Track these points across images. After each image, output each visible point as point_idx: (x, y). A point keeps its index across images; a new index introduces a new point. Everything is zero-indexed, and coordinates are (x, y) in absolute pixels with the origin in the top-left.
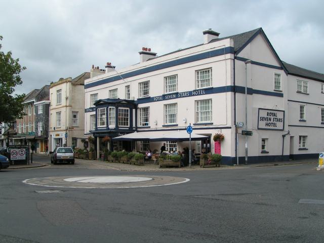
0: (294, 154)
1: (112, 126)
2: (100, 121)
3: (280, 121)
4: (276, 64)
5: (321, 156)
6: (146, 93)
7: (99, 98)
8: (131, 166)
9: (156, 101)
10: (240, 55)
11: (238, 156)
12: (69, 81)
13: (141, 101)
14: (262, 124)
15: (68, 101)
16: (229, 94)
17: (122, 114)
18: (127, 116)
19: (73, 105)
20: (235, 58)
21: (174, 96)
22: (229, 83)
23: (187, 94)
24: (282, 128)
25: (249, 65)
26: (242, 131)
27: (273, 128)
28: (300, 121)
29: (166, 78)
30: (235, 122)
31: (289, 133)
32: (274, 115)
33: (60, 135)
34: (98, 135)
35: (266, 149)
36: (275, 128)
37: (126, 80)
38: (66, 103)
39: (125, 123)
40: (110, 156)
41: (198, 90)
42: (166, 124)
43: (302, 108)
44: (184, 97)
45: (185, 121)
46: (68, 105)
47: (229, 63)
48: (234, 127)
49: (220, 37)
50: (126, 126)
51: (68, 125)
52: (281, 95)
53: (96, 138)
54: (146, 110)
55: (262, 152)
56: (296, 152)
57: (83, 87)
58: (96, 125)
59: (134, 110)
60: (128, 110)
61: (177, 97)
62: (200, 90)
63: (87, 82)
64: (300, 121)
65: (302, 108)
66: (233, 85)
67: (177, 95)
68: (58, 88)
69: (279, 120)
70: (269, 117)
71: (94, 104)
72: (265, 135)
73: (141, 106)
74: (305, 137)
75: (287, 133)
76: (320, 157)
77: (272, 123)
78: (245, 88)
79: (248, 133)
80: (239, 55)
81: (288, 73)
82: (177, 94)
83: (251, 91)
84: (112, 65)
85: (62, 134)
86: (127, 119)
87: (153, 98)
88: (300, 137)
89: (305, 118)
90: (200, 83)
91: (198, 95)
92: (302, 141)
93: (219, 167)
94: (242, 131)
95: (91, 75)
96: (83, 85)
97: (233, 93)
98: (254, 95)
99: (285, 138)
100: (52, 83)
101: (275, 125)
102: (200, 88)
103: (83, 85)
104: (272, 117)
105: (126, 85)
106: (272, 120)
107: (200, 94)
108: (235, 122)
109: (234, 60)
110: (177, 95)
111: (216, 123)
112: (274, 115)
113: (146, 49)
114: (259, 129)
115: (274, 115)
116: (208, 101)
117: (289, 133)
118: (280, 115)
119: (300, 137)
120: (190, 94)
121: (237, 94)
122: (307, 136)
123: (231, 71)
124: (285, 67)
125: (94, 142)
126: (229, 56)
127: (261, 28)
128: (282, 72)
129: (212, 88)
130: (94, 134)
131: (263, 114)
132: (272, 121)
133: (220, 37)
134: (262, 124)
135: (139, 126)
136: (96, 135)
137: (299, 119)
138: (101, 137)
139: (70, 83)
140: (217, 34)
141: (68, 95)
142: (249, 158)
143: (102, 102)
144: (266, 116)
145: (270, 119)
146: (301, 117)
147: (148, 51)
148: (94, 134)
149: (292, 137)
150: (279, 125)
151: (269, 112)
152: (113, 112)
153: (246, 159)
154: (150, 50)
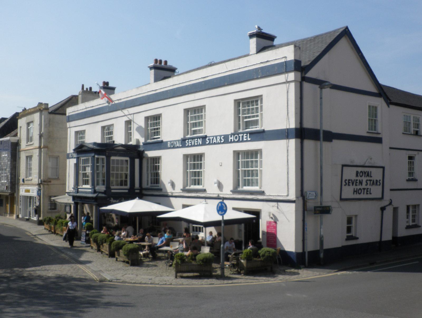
3: (376, 184)
4: (373, 89)
14: (348, 192)
20: (304, 79)
21: (200, 141)
23: (221, 140)
24: (380, 196)
25: (327, 91)
27: (365, 196)
28: (408, 180)
31: (391, 204)
32: (368, 175)
33: (31, 191)
35: (353, 233)
36: (369, 196)
37: (126, 111)
44: (215, 144)
52: (379, 140)
54: (157, 160)
55: (349, 238)
56: (402, 232)
59: (137, 161)
61: (204, 144)
62: (243, 133)
64: (408, 180)
68: (29, 118)
69: (375, 183)
70: (359, 178)
74: (416, 207)
75: (387, 203)
77: (364, 189)
79: (325, 210)
80: (311, 74)
81: (389, 102)
82: (204, 138)
84: (110, 85)
85: (33, 190)
87: (167, 142)
91: (238, 141)
95: (80, 100)
97: (299, 140)
98: (335, 142)
99: (385, 211)
100: (25, 110)
101: (368, 191)
104: (364, 179)
105: (126, 119)
106: (364, 183)
107: (243, 141)
111: (270, 192)
114: (341, 199)
115: (368, 174)
116: (255, 153)
117: (391, 204)
118: (376, 174)
119: (408, 207)
120: (226, 140)
124: (385, 93)
127: (347, 28)
128: (379, 102)
129: (263, 131)
131: (350, 174)
132: (364, 186)
134: (348, 192)
135: (145, 185)
142: (328, 251)
144: (353, 177)
145: (361, 183)
150: (376, 191)
151: (360, 169)
153: (322, 255)
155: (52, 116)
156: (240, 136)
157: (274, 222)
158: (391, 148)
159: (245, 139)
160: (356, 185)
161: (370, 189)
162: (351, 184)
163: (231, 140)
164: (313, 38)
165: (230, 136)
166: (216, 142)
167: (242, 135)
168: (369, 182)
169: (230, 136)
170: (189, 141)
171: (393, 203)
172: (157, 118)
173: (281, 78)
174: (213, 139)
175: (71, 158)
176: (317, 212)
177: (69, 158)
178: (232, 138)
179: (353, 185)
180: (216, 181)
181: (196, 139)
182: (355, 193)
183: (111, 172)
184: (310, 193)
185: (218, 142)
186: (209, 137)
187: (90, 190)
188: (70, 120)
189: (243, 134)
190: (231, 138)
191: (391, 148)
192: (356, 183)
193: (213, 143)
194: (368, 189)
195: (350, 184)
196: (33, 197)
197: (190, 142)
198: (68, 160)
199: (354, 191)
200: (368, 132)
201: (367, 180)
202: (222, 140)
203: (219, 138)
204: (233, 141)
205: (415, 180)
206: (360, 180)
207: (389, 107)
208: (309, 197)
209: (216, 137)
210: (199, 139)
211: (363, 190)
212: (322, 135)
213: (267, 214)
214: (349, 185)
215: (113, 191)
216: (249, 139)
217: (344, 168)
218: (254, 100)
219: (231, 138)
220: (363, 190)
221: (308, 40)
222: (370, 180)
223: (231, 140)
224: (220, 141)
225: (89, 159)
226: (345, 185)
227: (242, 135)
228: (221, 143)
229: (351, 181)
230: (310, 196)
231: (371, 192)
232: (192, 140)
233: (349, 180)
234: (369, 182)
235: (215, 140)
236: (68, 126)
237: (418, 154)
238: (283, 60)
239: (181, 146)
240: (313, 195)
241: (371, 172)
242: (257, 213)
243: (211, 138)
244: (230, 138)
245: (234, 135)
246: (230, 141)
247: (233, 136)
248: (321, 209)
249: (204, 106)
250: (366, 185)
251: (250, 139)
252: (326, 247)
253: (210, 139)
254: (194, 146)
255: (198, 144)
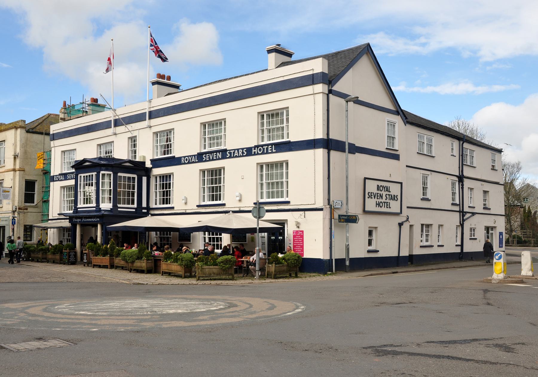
0: (414, 253)
1: (106, 206)
2: (82, 197)
5: (497, 257)
6: (168, 148)
7: (79, 157)
8: (48, 264)
9: (185, 164)
10: (337, 87)
11: (334, 258)
12: (21, 127)
13: (156, 163)
15: (18, 161)
16: (320, 152)
17: (124, 185)
18: (134, 189)
19: (27, 168)
20: (330, 91)
21: (220, 155)
22: (320, 135)
23: (243, 153)
24: (399, 211)
26: (339, 216)
29: (204, 125)
30: (329, 200)
31: (408, 219)
32: (387, 190)
34: (78, 220)
38: (15, 164)
39: (128, 200)
40: (49, 253)
41: (262, 146)
42: (63, 212)
43: (425, 178)
44: (236, 157)
45: (238, 198)
46: (17, 167)
47: (320, 99)
48: (327, 211)
49: (294, 58)
50: (130, 206)
51: (16, 204)
52: (396, 157)
53: (74, 226)
54: (166, 178)
56: (417, 251)
57: (47, 138)
58: (76, 202)
59: (144, 179)
60: (134, 178)
61: (224, 157)
62: (268, 145)
63: (54, 129)
65: (425, 178)
66: (326, 137)
67: (224, 154)
69: (394, 198)
71: (73, 167)
72: (373, 221)
73: (157, 171)
75: (405, 219)
76: (495, 260)
77: (385, 202)
78: (345, 143)
79: (351, 219)
80: (336, 88)
82: (224, 151)
83: (354, 149)
86: (133, 194)
88: (422, 225)
89: (428, 196)
90: (266, 134)
91: (263, 153)
92: (424, 234)
93: (296, 277)
94: (339, 216)
96: (48, 134)
97: (326, 151)
101: (388, 206)
102: (266, 142)
103: (48, 134)
104: (384, 193)
105: (130, 135)
106: (384, 197)
107: (267, 153)
108: (329, 200)
109: (328, 95)
110: (224, 154)
111: (295, 201)
112: (387, 189)
113: (163, 77)
116: (279, 165)
118: (395, 190)
119: (422, 225)
120: (249, 152)
121: (332, 153)
122: (431, 225)
123: (323, 114)
125: (72, 231)
126: (320, 88)
128: (397, 120)
129: (289, 142)
130: (71, 218)
133: (294, 58)
134: (371, 205)
135: (153, 205)
136: (75, 220)
137: (422, 197)
138: (83, 225)
139: (24, 131)
140: (290, 55)
141: (18, 150)
142: (352, 260)
143: (87, 164)
144: (375, 191)
145: (381, 197)
146: (424, 194)
147: (165, 81)
148: (71, 218)
149: (411, 226)
150: (395, 207)
152: (107, 183)
153: (347, 263)
154: (169, 78)
155: (30, 135)
156: (264, 148)
157: (299, 236)
158: (407, 166)
159: (215, 158)
160: (378, 198)
161: (389, 203)
162: (373, 197)
163: (255, 152)
164: (334, 54)
165: (253, 148)
166: (238, 155)
167: (267, 147)
168: (388, 196)
169: (253, 148)
170: (206, 155)
171: (409, 220)
172: (170, 131)
173: (308, 90)
174: (234, 153)
175: (56, 181)
176: (342, 220)
177: (54, 181)
178: (256, 151)
179: (375, 198)
180: (237, 194)
181: (215, 153)
182: (377, 206)
183: (118, 189)
184: (336, 202)
185: (240, 155)
186: (230, 150)
187: (95, 209)
188: (55, 138)
189: (268, 146)
190: (255, 151)
191: (407, 166)
192: (378, 196)
193: (235, 156)
194: (387, 203)
195: (372, 197)
196: (328, 68)
197: (70, 176)
198: (52, 183)
199: (377, 204)
200: (387, 149)
201: (386, 195)
202: (244, 153)
203: (241, 151)
204: (256, 153)
205: (428, 200)
206: (380, 194)
207: (405, 125)
208: (335, 206)
209: (238, 150)
210: (218, 153)
211: (383, 204)
212: (347, 147)
213: (294, 224)
214: (372, 198)
215: (119, 209)
216: (274, 151)
217: (367, 180)
218: (280, 112)
219: (255, 151)
220: (383, 204)
221: (330, 56)
222: (389, 195)
223: (255, 152)
224: (243, 155)
225: (92, 175)
226: (368, 198)
227: (267, 147)
228: (243, 156)
229: (372, 194)
230: (337, 205)
231: (390, 207)
232: (210, 154)
233: (371, 193)
234: (388, 196)
235: (236, 154)
236: (52, 145)
237: (431, 174)
238: (311, 73)
239: (197, 161)
240: (339, 204)
241: (389, 187)
242: (282, 223)
243: (232, 151)
244: (253, 151)
245: (258, 148)
246: (253, 153)
247: (256, 148)
248: (346, 218)
249: (225, 120)
250: (386, 199)
251: (275, 151)
252: (351, 256)
253: (231, 152)
254: (213, 160)
255: (217, 158)
